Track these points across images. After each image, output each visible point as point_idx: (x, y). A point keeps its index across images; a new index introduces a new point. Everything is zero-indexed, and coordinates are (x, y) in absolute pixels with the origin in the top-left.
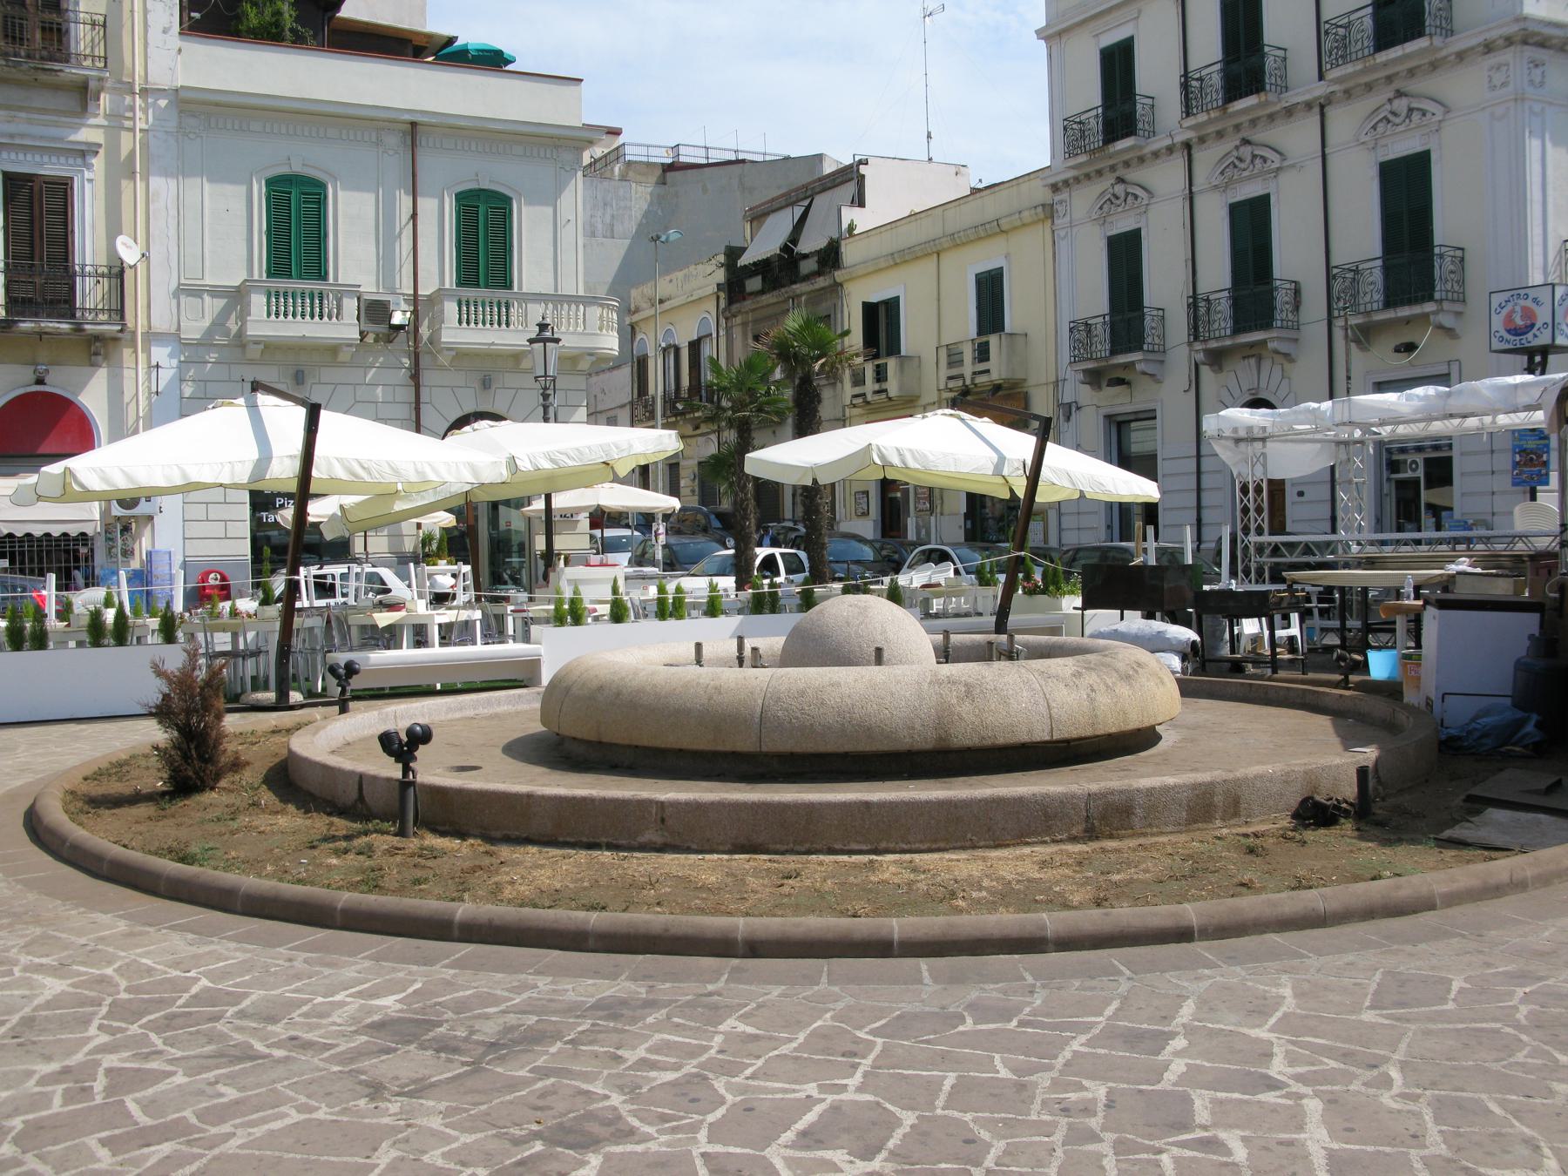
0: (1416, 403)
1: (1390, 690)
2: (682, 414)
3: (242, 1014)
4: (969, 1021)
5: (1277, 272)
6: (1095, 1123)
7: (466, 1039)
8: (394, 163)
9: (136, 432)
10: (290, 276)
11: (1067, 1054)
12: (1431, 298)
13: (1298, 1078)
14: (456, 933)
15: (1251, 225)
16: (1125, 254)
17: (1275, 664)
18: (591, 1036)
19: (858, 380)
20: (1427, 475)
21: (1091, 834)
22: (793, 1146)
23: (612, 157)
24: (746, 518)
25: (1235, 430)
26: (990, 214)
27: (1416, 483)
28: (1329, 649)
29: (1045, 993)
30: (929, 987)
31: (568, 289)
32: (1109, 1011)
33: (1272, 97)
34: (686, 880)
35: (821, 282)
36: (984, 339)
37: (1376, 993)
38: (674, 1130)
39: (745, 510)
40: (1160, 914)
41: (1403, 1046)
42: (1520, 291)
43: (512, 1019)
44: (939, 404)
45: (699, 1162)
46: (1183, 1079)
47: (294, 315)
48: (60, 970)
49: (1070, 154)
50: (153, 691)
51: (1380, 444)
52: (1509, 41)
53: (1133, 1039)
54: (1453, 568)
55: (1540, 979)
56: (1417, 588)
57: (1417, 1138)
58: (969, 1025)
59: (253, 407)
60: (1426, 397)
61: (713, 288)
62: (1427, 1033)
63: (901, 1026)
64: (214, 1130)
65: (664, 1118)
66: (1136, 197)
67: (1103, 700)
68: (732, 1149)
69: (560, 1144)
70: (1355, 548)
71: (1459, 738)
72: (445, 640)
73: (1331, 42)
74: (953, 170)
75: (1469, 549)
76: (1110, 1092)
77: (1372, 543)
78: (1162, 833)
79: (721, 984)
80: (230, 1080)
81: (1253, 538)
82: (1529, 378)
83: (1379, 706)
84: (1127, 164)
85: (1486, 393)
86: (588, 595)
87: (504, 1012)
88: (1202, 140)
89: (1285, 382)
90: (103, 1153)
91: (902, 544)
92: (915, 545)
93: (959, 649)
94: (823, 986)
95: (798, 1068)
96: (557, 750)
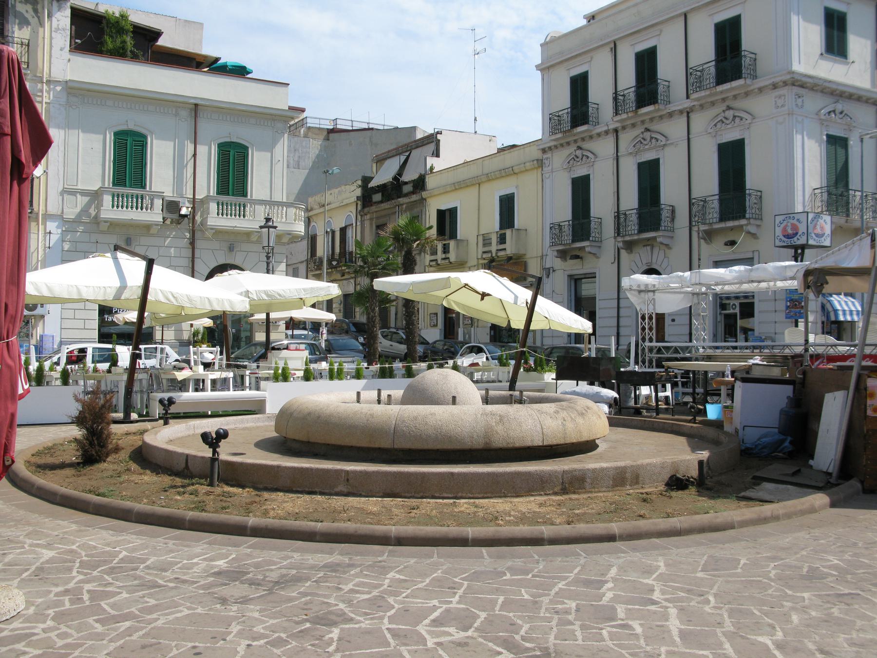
0: (734, 274)
1: (717, 424)
2: (335, 267)
3: (148, 567)
4: (508, 574)
5: (663, 200)
6: (571, 617)
7: (263, 580)
8: (186, 126)
9: (36, 269)
10: (125, 186)
11: (556, 589)
12: (744, 217)
13: (666, 600)
14: (249, 532)
15: (649, 174)
16: (581, 189)
17: (658, 410)
18: (325, 579)
19: (434, 252)
20: (740, 312)
21: (564, 491)
22: (429, 625)
23: (300, 124)
24: (374, 326)
25: (639, 286)
26: (508, 164)
27: (734, 316)
28: (686, 403)
29: (544, 563)
30: (487, 560)
31: (278, 197)
32: (576, 571)
33: (662, 107)
34: (362, 509)
35: (414, 198)
36: (503, 232)
37: (704, 565)
38: (372, 619)
39: (374, 322)
40: (599, 528)
41: (716, 587)
42: (790, 215)
43: (284, 571)
44: (477, 267)
45: (386, 632)
46: (612, 600)
47: (127, 207)
48: (49, 546)
49: (553, 133)
50: (74, 409)
51: (716, 295)
52: (785, 84)
53: (588, 583)
54: (751, 362)
55: (782, 559)
56: (733, 373)
57: (720, 624)
58: (508, 576)
59: (115, 259)
60: (740, 271)
61: (354, 199)
62: (728, 582)
63: (475, 577)
64: (149, 617)
65: (366, 614)
66: (588, 157)
67: (570, 425)
68: (400, 627)
69: (318, 624)
70: (701, 350)
71: (751, 449)
72: (214, 389)
73: (693, 79)
74: (488, 138)
75: (761, 352)
76: (577, 605)
77: (710, 348)
78: (600, 492)
79: (385, 557)
80: (151, 595)
81: (647, 344)
82: (793, 263)
83: (711, 432)
84: (583, 139)
85: (770, 269)
86: (291, 365)
87: (279, 568)
88: (624, 128)
89: (666, 260)
90: (97, 625)
91: (456, 343)
92: (463, 343)
93: (492, 398)
94: (435, 558)
95: (427, 593)
96: (284, 445)
